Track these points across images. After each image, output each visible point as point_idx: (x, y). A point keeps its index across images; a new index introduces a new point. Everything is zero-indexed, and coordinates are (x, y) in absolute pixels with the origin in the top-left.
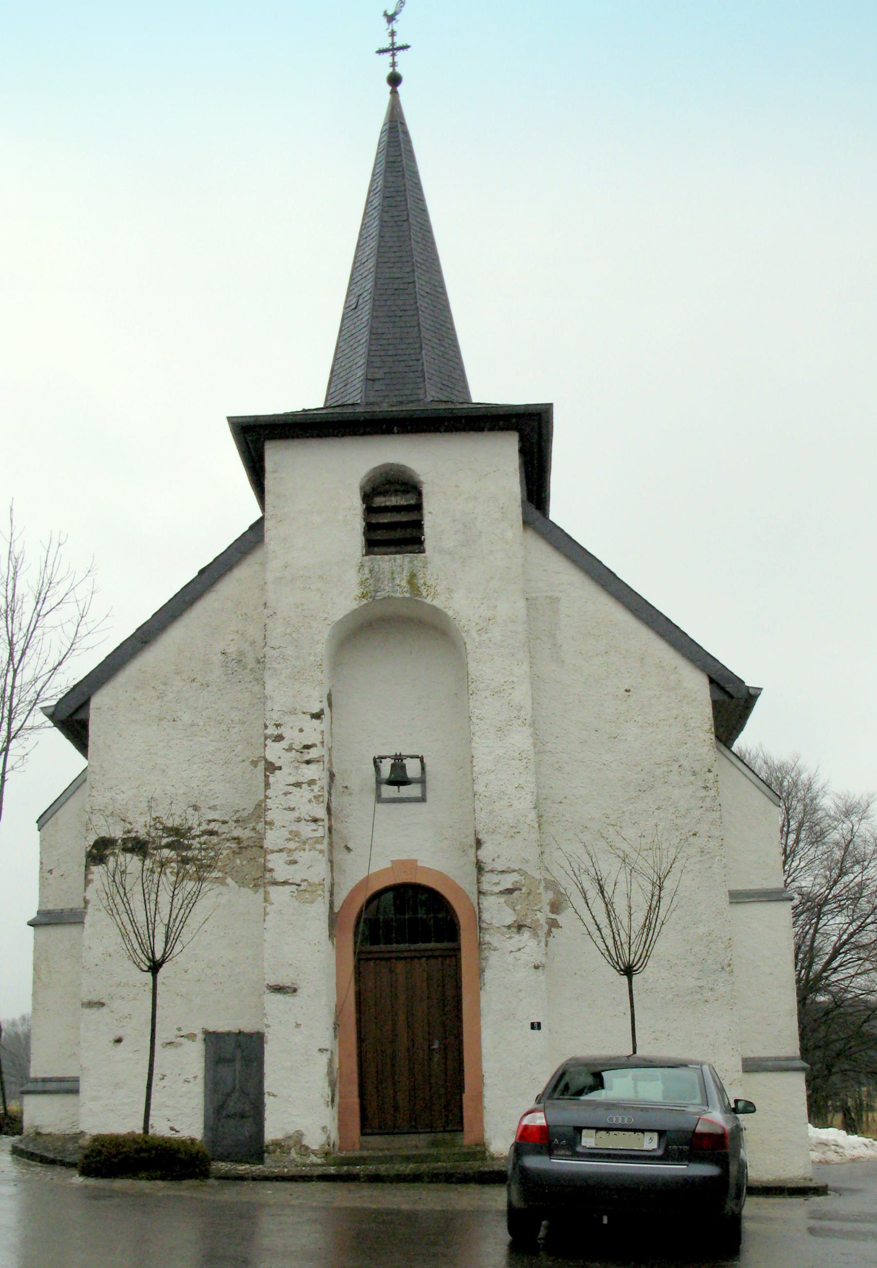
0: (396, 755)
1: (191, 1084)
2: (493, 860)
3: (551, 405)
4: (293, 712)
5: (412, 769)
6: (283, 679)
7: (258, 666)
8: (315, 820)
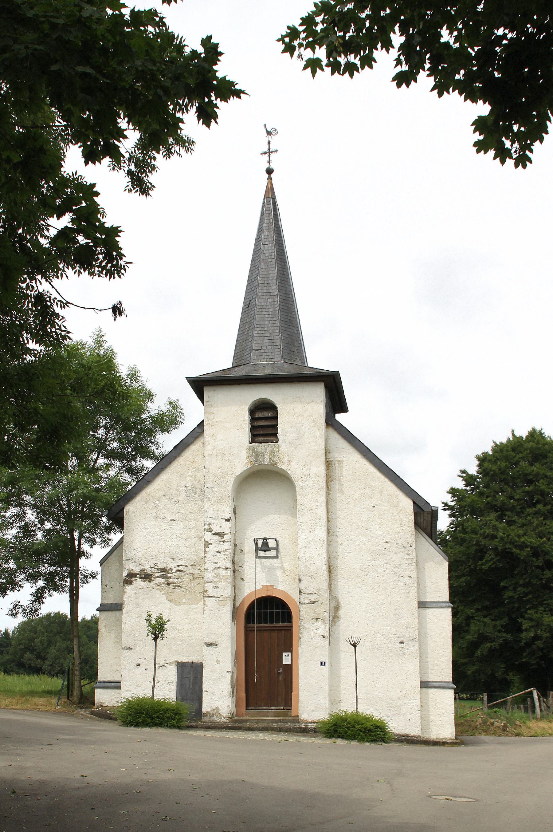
0: (264, 538)
4: (217, 518)
5: (272, 544)
8: (227, 569)
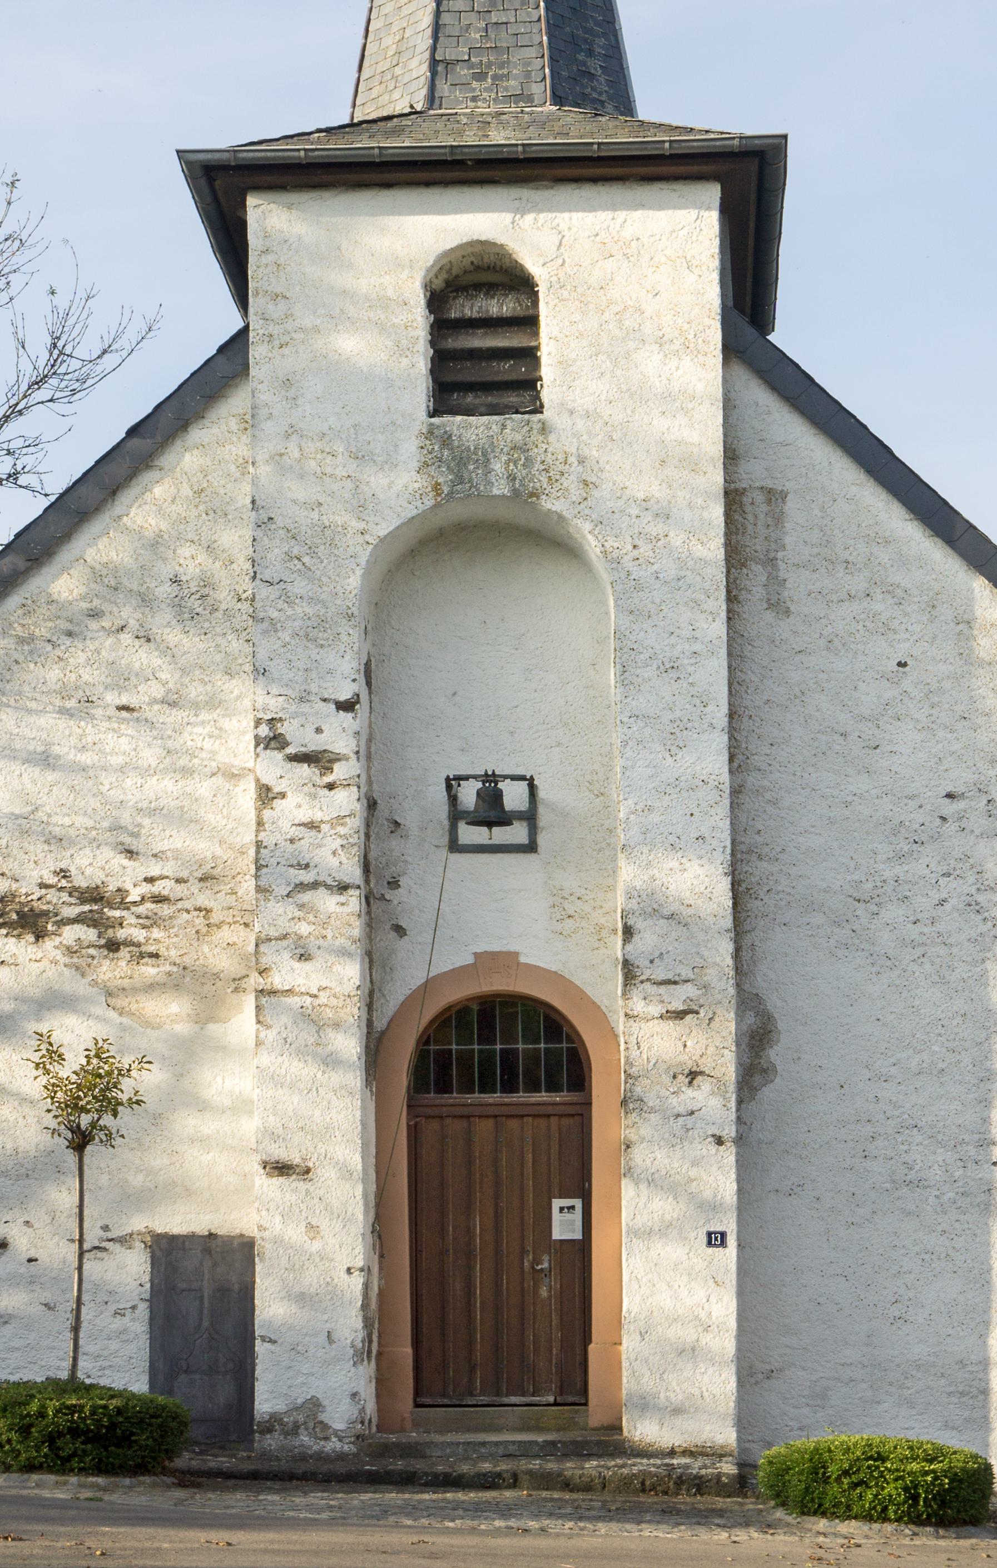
0: (486, 775)
1: (126, 1320)
2: (652, 962)
3: (785, 137)
5: (514, 796)
6: (287, 639)
7: (239, 605)
